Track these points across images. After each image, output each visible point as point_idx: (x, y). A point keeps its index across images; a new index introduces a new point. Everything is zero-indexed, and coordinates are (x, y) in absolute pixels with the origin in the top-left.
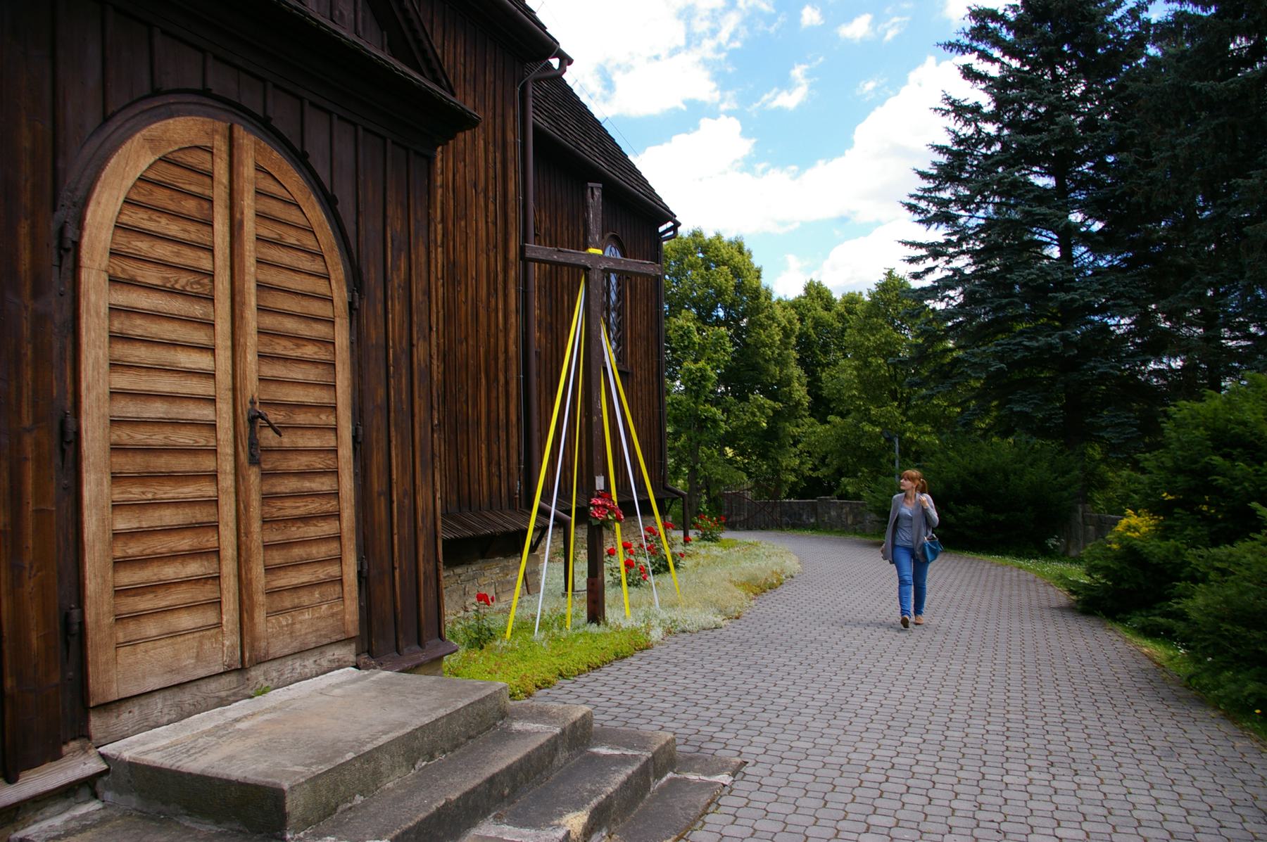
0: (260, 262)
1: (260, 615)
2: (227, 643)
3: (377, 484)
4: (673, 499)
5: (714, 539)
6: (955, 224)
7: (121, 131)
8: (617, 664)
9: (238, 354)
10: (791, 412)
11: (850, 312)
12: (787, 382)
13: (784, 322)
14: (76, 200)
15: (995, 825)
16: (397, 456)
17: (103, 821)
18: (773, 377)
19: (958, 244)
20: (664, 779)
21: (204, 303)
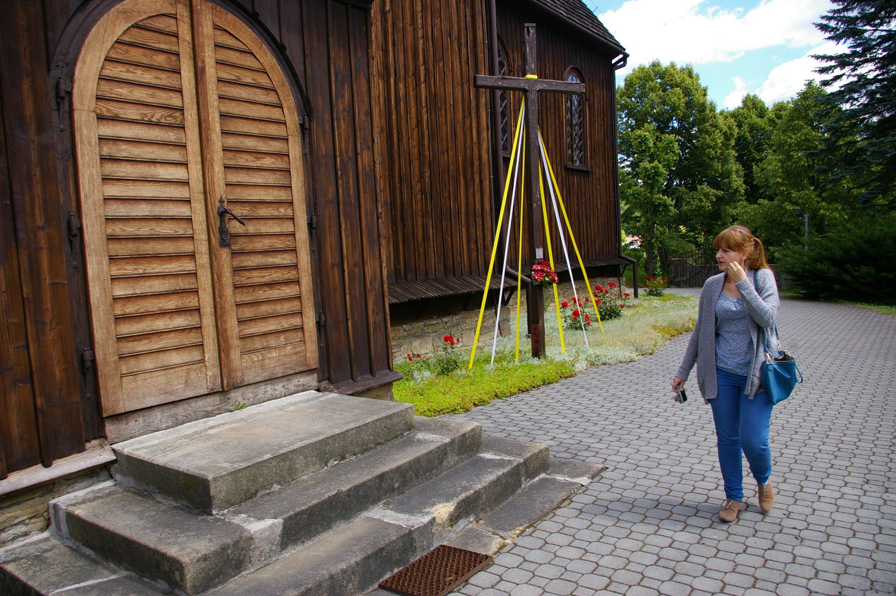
0: (221, 97)
1: (235, 355)
2: (210, 373)
3: (330, 258)
4: (626, 265)
5: (659, 295)
6: (860, 38)
7: (101, 7)
8: (543, 388)
9: (206, 167)
10: (731, 197)
11: (779, 117)
12: (727, 174)
13: (725, 129)
14: (68, 61)
15: (796, 532)
16: (347, 237)
17: (110, 494)
18: (716, 171)
19: (863, 54)
20: (537, 479)
21: (176, 131)
